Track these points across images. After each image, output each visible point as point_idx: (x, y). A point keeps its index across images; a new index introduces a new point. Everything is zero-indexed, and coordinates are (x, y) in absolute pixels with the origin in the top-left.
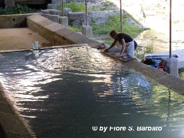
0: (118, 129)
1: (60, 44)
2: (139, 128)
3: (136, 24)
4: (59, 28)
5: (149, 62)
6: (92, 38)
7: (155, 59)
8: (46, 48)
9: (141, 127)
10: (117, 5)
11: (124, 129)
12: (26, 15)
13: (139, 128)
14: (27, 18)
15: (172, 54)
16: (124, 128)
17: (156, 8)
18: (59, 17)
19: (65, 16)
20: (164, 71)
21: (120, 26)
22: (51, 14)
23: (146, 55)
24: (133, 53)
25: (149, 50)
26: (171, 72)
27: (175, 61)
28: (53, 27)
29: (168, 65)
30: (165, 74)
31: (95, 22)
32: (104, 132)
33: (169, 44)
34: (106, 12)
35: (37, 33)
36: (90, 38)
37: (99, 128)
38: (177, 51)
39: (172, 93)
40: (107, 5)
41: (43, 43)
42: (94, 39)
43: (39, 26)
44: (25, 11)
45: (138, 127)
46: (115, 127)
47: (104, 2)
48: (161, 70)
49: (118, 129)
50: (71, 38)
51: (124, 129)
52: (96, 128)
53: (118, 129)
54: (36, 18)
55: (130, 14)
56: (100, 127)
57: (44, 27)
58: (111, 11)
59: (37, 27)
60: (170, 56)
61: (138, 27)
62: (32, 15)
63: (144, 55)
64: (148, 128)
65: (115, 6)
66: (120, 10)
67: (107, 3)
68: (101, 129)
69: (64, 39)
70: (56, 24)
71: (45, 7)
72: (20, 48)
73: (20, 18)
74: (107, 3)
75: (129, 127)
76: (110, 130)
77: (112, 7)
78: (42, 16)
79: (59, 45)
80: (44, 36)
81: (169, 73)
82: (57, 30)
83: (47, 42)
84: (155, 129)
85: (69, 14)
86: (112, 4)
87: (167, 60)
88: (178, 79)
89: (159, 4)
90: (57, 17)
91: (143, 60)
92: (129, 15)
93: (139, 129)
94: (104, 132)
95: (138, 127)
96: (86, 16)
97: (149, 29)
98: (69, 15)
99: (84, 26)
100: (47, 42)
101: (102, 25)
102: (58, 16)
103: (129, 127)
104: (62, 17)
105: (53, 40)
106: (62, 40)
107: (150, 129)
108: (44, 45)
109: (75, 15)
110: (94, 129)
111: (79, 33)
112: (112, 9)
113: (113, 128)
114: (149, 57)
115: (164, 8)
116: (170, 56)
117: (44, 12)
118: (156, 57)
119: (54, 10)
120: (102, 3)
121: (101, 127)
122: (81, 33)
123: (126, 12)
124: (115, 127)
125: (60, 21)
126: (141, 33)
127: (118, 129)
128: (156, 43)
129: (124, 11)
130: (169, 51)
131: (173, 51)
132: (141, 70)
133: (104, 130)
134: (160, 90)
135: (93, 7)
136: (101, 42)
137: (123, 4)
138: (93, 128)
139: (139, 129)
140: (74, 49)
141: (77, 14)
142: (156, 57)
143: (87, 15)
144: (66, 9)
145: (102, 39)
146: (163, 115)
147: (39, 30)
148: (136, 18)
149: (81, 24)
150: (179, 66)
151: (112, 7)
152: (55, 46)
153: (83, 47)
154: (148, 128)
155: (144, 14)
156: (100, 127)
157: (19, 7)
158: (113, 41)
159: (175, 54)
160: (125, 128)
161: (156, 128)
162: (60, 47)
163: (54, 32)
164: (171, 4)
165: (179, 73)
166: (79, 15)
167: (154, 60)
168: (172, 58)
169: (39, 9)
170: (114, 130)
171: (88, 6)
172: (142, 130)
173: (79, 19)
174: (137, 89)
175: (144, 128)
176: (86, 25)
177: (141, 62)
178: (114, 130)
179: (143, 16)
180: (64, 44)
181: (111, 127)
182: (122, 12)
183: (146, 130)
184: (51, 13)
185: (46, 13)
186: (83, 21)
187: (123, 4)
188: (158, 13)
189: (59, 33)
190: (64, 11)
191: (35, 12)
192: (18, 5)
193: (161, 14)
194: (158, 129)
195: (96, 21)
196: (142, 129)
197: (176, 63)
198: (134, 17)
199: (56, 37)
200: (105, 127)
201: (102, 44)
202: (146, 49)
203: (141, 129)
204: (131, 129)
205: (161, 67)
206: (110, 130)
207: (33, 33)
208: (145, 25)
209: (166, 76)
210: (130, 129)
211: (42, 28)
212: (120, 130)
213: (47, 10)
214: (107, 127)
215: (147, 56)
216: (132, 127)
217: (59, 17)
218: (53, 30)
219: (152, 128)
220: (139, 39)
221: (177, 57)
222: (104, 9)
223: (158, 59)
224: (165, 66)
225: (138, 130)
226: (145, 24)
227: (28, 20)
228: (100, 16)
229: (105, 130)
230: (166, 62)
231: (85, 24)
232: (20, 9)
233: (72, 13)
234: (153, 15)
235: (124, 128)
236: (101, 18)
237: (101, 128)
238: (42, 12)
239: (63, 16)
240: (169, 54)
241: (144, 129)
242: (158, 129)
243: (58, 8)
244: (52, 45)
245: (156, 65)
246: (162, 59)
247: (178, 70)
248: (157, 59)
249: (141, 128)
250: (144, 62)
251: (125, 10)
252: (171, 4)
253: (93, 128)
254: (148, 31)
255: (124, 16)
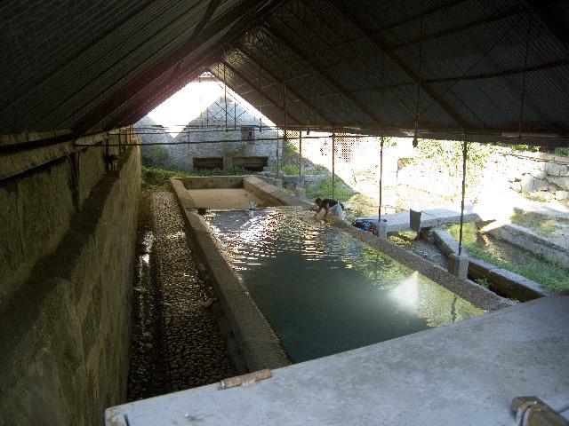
5: (359, 225)
6: (305, 201)
24: (343, 215)
25: (359, 214)
28: (269, 188)
35: (241, 236)
43: (253, 186)
50: (284, 199)
54: (252, 179)
73: (237, 179)
80: (260, 197)
83: (262, 203)
98: (283, 178)
100: (262, 203)
105: (266, 201)
146: (381, 269)
147: (255, 190)
148: (348, 183)
158: (472, 144)
163: (269, 194)
184: (266, 175)
189: (273, 194)
197: (384, 227)
198: (346, 182)
208: (356, 189)
218: (269, 192)
222: (317, 174)
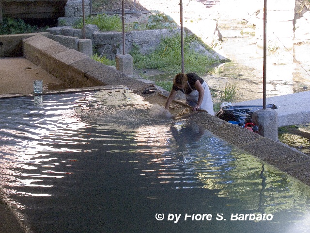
0: (198, 217)
1: (80, 85)
2: (234, 216)
3: (207, 52)
4: (80, 59)
5: (228, 116)
7: (238, 111)
8: (56, 92)
9: (237, 214)
10: (175, 20)
11: (209, 218)
12: (21, 37)
13: (234, 216)
14: (24, 40)
15: (267, 103)
16: (209, 217)
17: (240, 26)
18: (77, 39)
19: (87, 38)
20: (254, 131)
21: (180, 56)
22: (64, 34)
23: (224, 105)
25: (229, 96)
26: (266, 132)
27: (272, 114)
28: (68, 56)
29: (260, 121)
30: (256, 137)
31: (138, 49)
32: (175, 222)
33: (262, 85)
34: (157, 31)
36: (130, 76)
37: (166, 217)
38: (275, 97)
39: (265, 166)
40: (159, 21)
41: (50, 84)
42: (135, 77)
43: (43, 54)
44: (20, 29)
45: (232, 214)
46: (194, 215)
47: (153, 15)
48: (249, 130)
49: (198, 217)
50: (97, 75)
51: (209, 218)
52: (162, 216)
53: (198, 217)
55: (197, 36)
56: (169, 214)
57: (53, 58)
58: (164, 30)
59: (40, 56)
60: (264, 106)
61: (210, 57)
62: (33, 36)
63: (219, 104)
64: (249, 216)
65: (172, 22)
66: (180, 28)
67: (158, 17)
68: (171, 217)
69: (85, 76)
70: (73, 51)
71: (53, 22)
72: (12, 92)
74: (158, 17)
75: (218, 215)
76: (185, 219)
77: (167, 24)
78: (49, 37)
79: (78, 87)
81: (262, 134)
82: (73, 62)
83: (57, 82)
84: (261, 217)
85: (93, 35)
86: (166, 19)
87: (258, 113)
88: (277, 145)
89: (244, 19)
90: (74, 40)
91: (219, 113)
92: (194, 37)
93: (234, 217)
94: (175, 222)
95: (232, 214)
96: (123, 38)
97: (229, 61)
98: (93, 37)
99: (119, 55)
100: (57, 82)
101: (149, 55)
102: (75, 38)
103: (218, 215)
104: (83, 40)
105: (67, 81)
106: (80, 78)
107: (252, 217)
108: (51, 87)
109: (105, 37)
110: (159, 217)
111: (111, 67)
112: (166, 28)
113: (190, 216)
114: (227, 107)
115: (254, 25)
116: (264, 106)
117: (51, 32)
118: (240, 108)
119: (68, 28)
120: (149, 17)
121: (170, 215)
122: (114, 67)
123: (190, 31)
124: (194, 215)
125: (79, 47)
126: (216, 68)
127: (198, 217)
128: (242, 85)
129: (187, 31)
130: (262, 98)
131: (268, 98)
132: (216, 130)
133: (175, 219)
134: (250, 162)
135: (134, 22)
136: (148, 82)
137: (186, 18)
138: (157, 216)
139: (234, 218)
140: (103, 94)
141: (108, 35)
142: (240, 108)
143: (125, 37)
144: (89, 26)
145: (150, 78)
148: (208, 42)
149: (115, 52)
150: (280, 124)
151: (167, 24)
152: (70, 88)
153: (118, 90)
154: (248, 217)
155: (220, 35)
156: (169, 214)
157: (10, 23)
159: (273, 102)
160: (211, 217)
161: (263, 216)
162: (78, 90)
163: (69, 66)
164: (265, 19)
165: (280, 135)
166: (112, 37)
167: (236, 113)
168: (268, 109)
169: (45, 26)
170: (193, 220)
171: (127, 22)
172: (239, 220)
173: (112, 43)
174: (12, 29)
175: (242, 216)
176: (124, 54)
177: (215, 117)
178: (193, 220)
179: (218, 38)
180: (86, 86)
181: (186, 214)
182: (184, 33)
183: (246, 220)
184: (64, 32)
185: (55, 33)
186: (117, 47)
187: (186, 18)
188: (244, 35)
190: (85, 30)
191: (36, 30)
192: (9, 19)
193: (248, 35)
194: (265, 218)
195: (139, 47)
196: (239, 218)
197: (273, 118)
199: (72, 74)
200: (176, 215)
201: (151, 86)
202: (223, 94)
203: (237, 217)
204: (220, 217)
205: (249, 125)
206: (185, 219)
207: (33, 67)
209: (256, 141)
210: (220, 218)
211: (50, 58)
212: (203, 220)
213: (58, 29)
214: (180, 215)
215: (224, 106)
216: (222, 214)
217: (77, 39)
219: (256, 216)
220: (211, 78)
221: (275, 107)
222: (153, 27)
223: (245, 112)
224: (256, 123)
225: (232, 219)
226: (221, 51)
227: (25, 46)
228: (147, 39)
229: (177, 219)
230: (257, 117)
231: (122, 53)
232: (12, 25)
233: (100, 33)
234: (236, 37)
235: (209, 217)
236: (147, 42)
237: (170, 217)
238: (47, 31)
239: (84, 38)
240: (261, 103)
241: (243, 218)
242: (265, 218)
243: (75, 25)
244: (65, 87)
245: (241, 121)
246: (250, 110)
247: (277, 130)
248: (243, 111)
249: (238, 216)
250: (220, 117)
251: (189, 28)
252: (265, 19)
253: (157, 216)
254: (227, 63)
255: (186, 38)
